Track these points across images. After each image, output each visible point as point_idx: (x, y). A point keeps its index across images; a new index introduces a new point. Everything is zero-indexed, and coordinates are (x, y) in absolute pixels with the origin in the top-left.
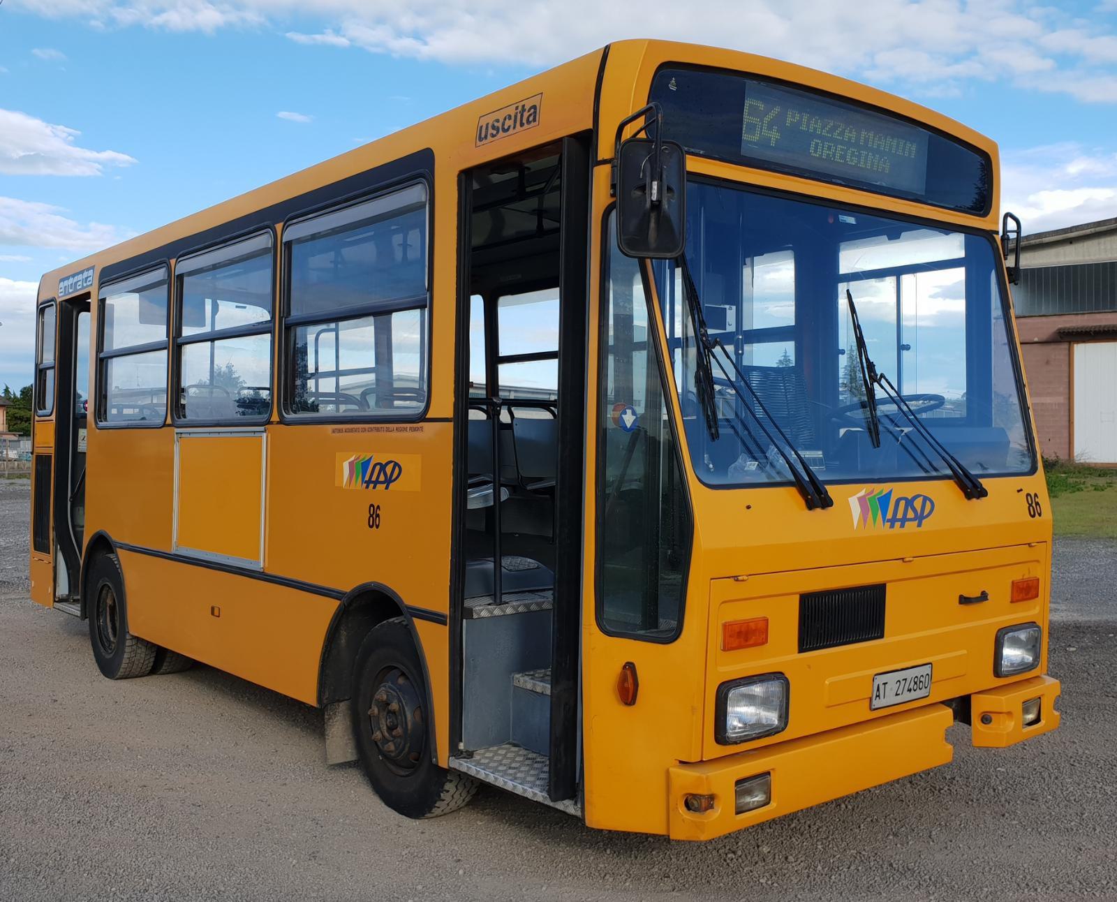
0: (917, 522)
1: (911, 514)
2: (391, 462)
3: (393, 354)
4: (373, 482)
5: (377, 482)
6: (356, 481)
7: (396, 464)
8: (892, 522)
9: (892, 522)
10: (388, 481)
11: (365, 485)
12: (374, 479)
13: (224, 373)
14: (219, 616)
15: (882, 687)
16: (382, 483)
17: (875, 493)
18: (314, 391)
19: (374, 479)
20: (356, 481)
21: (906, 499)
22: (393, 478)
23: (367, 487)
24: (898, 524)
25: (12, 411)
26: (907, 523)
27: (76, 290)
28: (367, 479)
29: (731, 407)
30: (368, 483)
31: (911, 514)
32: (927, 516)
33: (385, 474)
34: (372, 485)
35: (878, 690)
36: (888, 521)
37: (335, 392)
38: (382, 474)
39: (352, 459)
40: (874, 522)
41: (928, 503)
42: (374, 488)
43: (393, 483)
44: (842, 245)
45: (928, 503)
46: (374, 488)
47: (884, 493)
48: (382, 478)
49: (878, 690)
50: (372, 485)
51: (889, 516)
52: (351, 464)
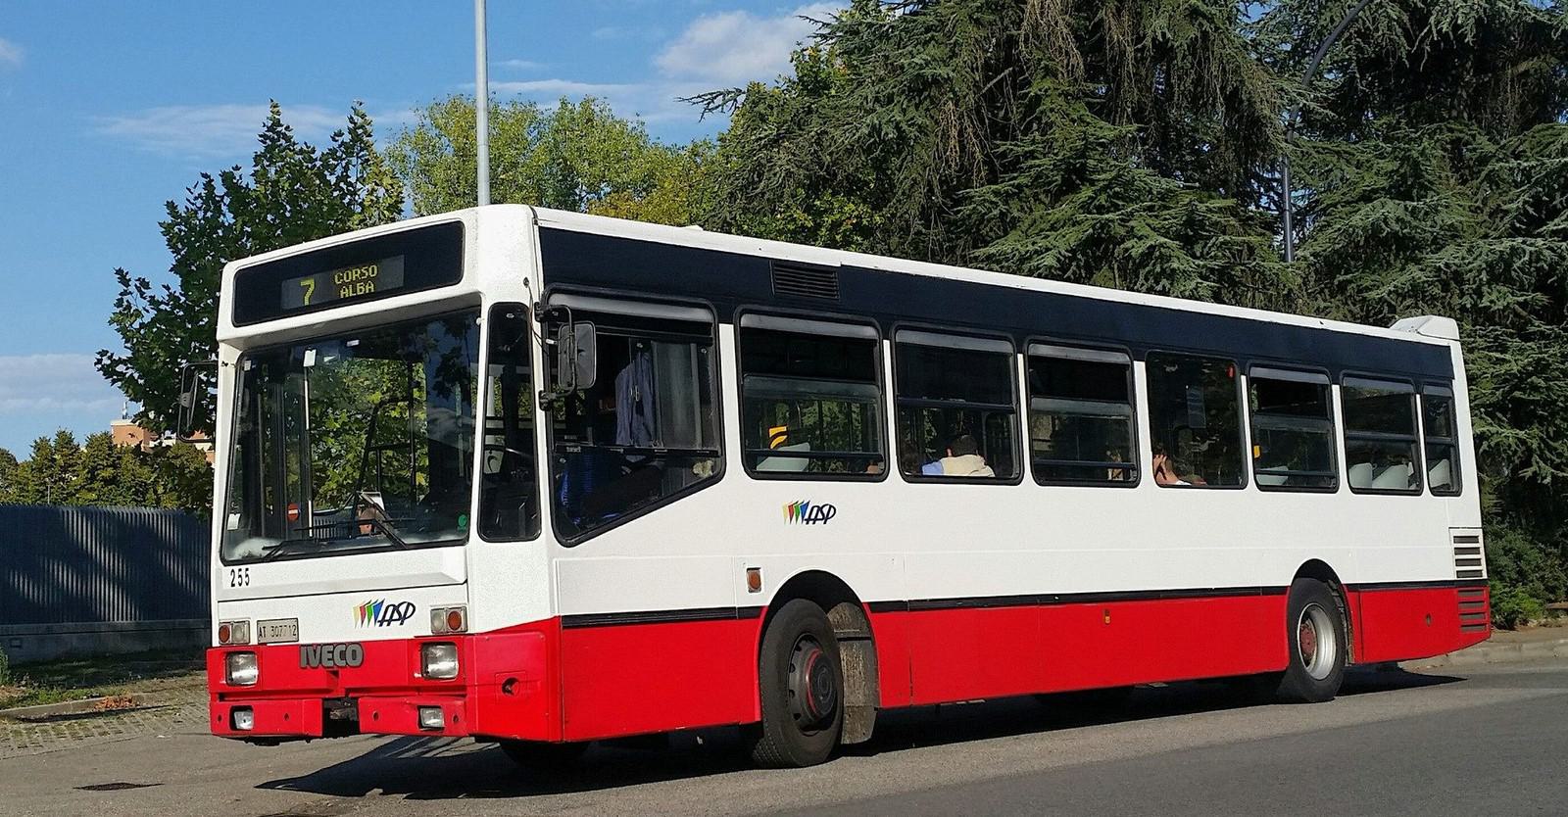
1: (820, 516)
9: (808, 521)
21: (394, 605)
23: (381, 625)
24: (385, 623)
31: (396, 616)
33: (399, 613)
42: (388, 625)
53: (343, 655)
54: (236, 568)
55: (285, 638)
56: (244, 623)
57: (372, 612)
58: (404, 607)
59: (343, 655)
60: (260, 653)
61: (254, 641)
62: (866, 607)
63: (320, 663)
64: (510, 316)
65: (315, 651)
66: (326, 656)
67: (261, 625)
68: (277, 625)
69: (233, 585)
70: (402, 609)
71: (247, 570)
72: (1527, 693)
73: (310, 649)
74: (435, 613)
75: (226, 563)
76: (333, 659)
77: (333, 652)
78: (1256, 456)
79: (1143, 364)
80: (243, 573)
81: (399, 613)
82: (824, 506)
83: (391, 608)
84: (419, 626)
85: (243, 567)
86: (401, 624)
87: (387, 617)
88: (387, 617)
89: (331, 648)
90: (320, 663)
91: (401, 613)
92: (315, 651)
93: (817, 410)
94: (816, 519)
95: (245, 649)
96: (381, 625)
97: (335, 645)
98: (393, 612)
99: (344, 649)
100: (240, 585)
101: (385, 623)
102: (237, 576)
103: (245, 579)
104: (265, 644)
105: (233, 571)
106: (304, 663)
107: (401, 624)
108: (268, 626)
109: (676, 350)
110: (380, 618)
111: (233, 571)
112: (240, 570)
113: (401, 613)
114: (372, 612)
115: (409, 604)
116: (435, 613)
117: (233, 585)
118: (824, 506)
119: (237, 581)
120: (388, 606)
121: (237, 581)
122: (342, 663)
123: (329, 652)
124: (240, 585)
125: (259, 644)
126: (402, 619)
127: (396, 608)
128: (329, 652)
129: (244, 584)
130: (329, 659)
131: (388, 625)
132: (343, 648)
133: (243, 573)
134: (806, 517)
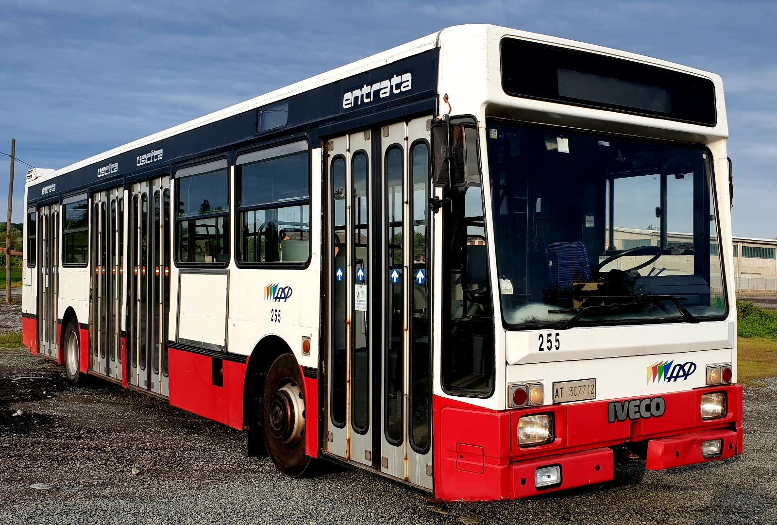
1: (681, 373)
3: (414, 192)
5: (280, 298)
9: (276, 298)
10: (286, 298)
11: (275, 299)
12: (279, 296)
14: (595, 379)
15: (560, 391)
16: (283, 298)
18: (54, 185)
19: (279, 296)
22: (689, 373)
23: (669, 381)
24: (673, 379)
25: (8, 225)
26: (678, 378)
28: (275, 296)
29: (439, 34)
30: (276, 298)
31: (681, 373)
33: (684, 371)
34: (278, 300)
35: (557, 391)
36: (668, 378)
38: (681, 371)
41: (290, 291)
42: (675, 380)
45: (290, 291)
46: (279, 301)
49: (557, 391)
50: (278, 300)
51: (668, 375)
53: (648, 408)
54: (545, 332)
55: (581, 399)
56: (539, 385)
57: (663, 371)
58: (287, 289)
59: (648, 408)
60: (555, 414)
61: (548, 401)
62: (366, 283)
63: (628, 415)
64: (704, 156)
65: (623, 407)
66: (633, 410)
67: (558, 386)
68: (575, 385)
69: (541, 349)
70: (686, 368)
71: (557, 335)
72: (483, 368)
73: (619, 406)
74: (709, 368)
75: (507, 327)
76: (639, 412)
77: (639, 406)
80: (553, 338)
81: (684, 371)
83: (678, 368)
84: (698, 380)
85: (553, 332)
86: (685, 379)
87: (675, 375)
88: (675, 375)
89: (638, 403)
90: (628, 415)
91: (685, 371)
92: (623, 407)
95: (538, 410)
96: (669, 381)
97: (641, 400)
99: (647, 402)
100: (549, 349)
102: (274, 315)
103: (555, 344)
104: (559, 403)
105: (541, 336)
106: (612, 419)
107: (685, 379)
108: (566, 386)
110: (668, 375)
111: (541, 336)
112: (549, 335)
113: (685, 371)
114: (663, 371)
115: (692, 364)
116: (709, 368)
117: (541, 349)
119: (545, 345)
121: (545, 345)
122: (648, 414)
123: (635, 406)
124: (549, 349)
125: (554, 404)
126: (686, 375)
127: (682, 367)
128: (635, 406)
129: (554, 348)
130: (635, 412)
131: (675, 380)
132: (648, 401)
133: (553, 338)
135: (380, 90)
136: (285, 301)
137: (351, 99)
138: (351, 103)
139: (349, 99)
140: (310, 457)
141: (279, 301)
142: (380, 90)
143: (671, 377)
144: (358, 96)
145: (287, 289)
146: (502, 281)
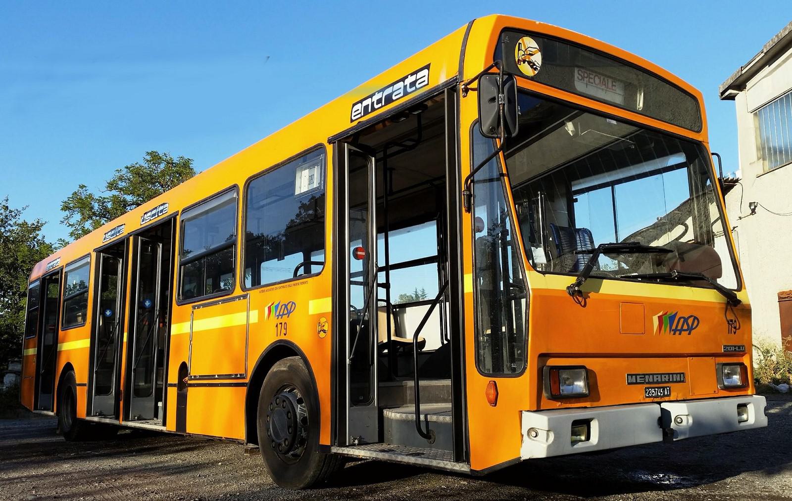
0: (688, 332)
1: (685, 327)
2: (691, 316)
4: (679, 330)
6: (665, 331)
7: (695, 318)
8: (675, 331)
9: (675, 331)
11: (672, 332)
12: (679, 328)
13: (53, 278)
16: (685, 330)
17: (668, 314)
19: (679, 328)
20: (665, 331)
21: (285, 305)
23: (674, 334)
24: (678, 333)
27: (53, 268)
30: (278, 316)
31: (685, 327)
32: (694, 329)
33: (688, 325)
34: (280, 317)
37: (385, 282)
39: (661, 314)
40: (665, 333)
42: (680, 334)
43: (694, 330)
44: (312, 253)
46: (680, 334)
47: (673, 314)
48: (286, 312)
50: (280, 317)
51: (674, 327)
52: (660, 318)
58: (692, 319)
78: (641, 398)
79: (490, 333)
81: (688, 325)
82: (288, 304)
86: (689, 334)
93: (322, 465)
94: (681, 331)
98: (684, 323)
101: (678, 333)
107: (689, 334)
109: (449, 405)
118: (288, 304)
120: (283, 305)
134: (674, 327)
135: (393, 92)
136: (288, 317)
137: (360, 110)
138: (361, 113)
139: (358, 110)
140: (409, 403)
141: (281, 318)
142: (393, 92)
143: (279, 315)
144: (369, 105)
145: (692, 319)
146: (262, 283)
